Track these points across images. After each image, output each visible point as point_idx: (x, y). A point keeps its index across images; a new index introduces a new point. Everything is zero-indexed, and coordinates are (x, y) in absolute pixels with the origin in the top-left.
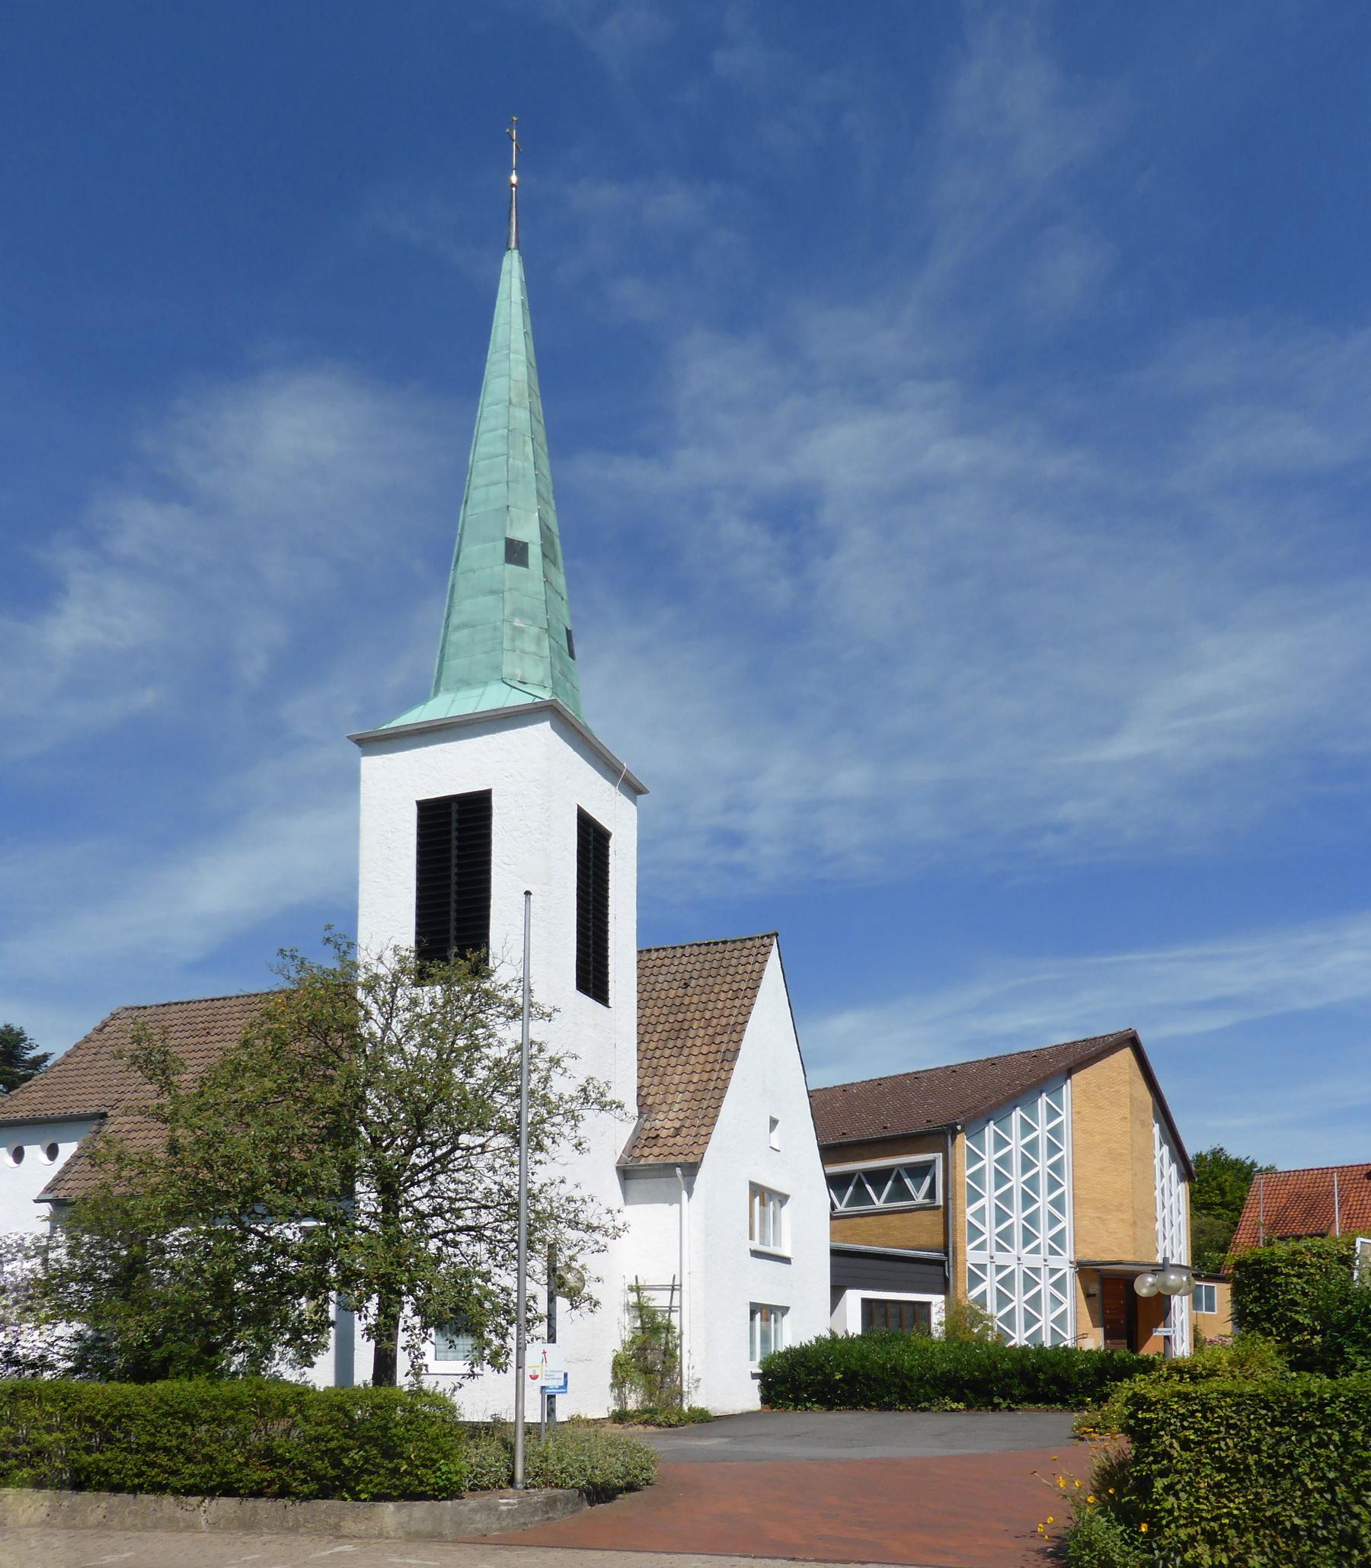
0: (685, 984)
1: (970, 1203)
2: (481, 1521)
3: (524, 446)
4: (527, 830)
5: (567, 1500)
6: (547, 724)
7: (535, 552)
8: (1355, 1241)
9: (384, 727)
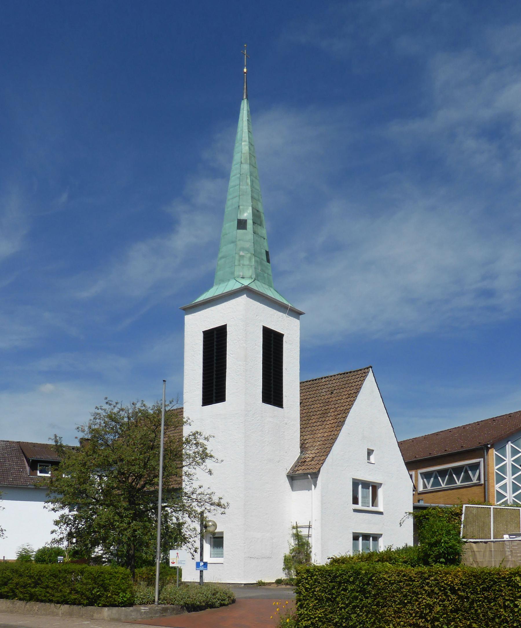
0: (332, 392)
1: (498, 482)
2: (134, 615)
3: (247, 180)
4: (238, 340)
5: (174, 609)
6: (245, 295)
7: (250, 223)
8: (463, 506)
9: (193, 303)
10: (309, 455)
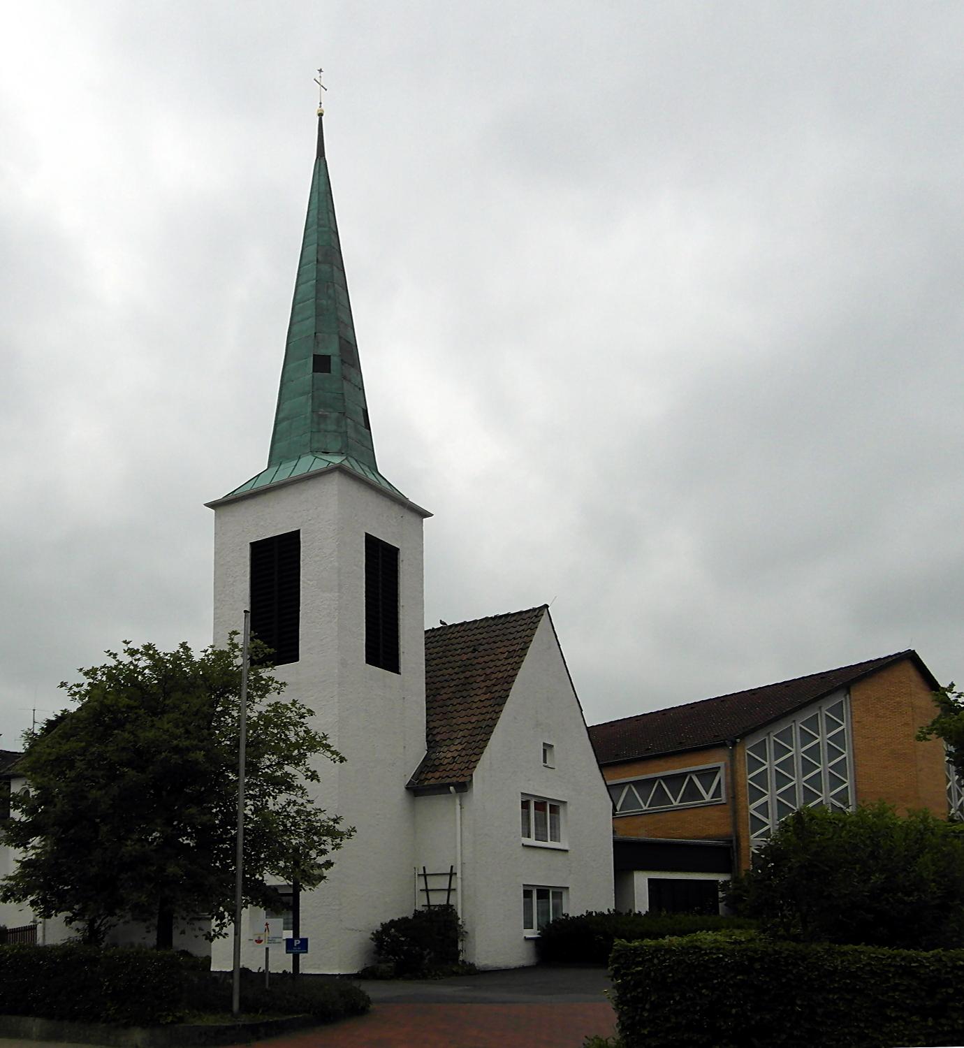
0: (474, 649)
10: (446, 754)
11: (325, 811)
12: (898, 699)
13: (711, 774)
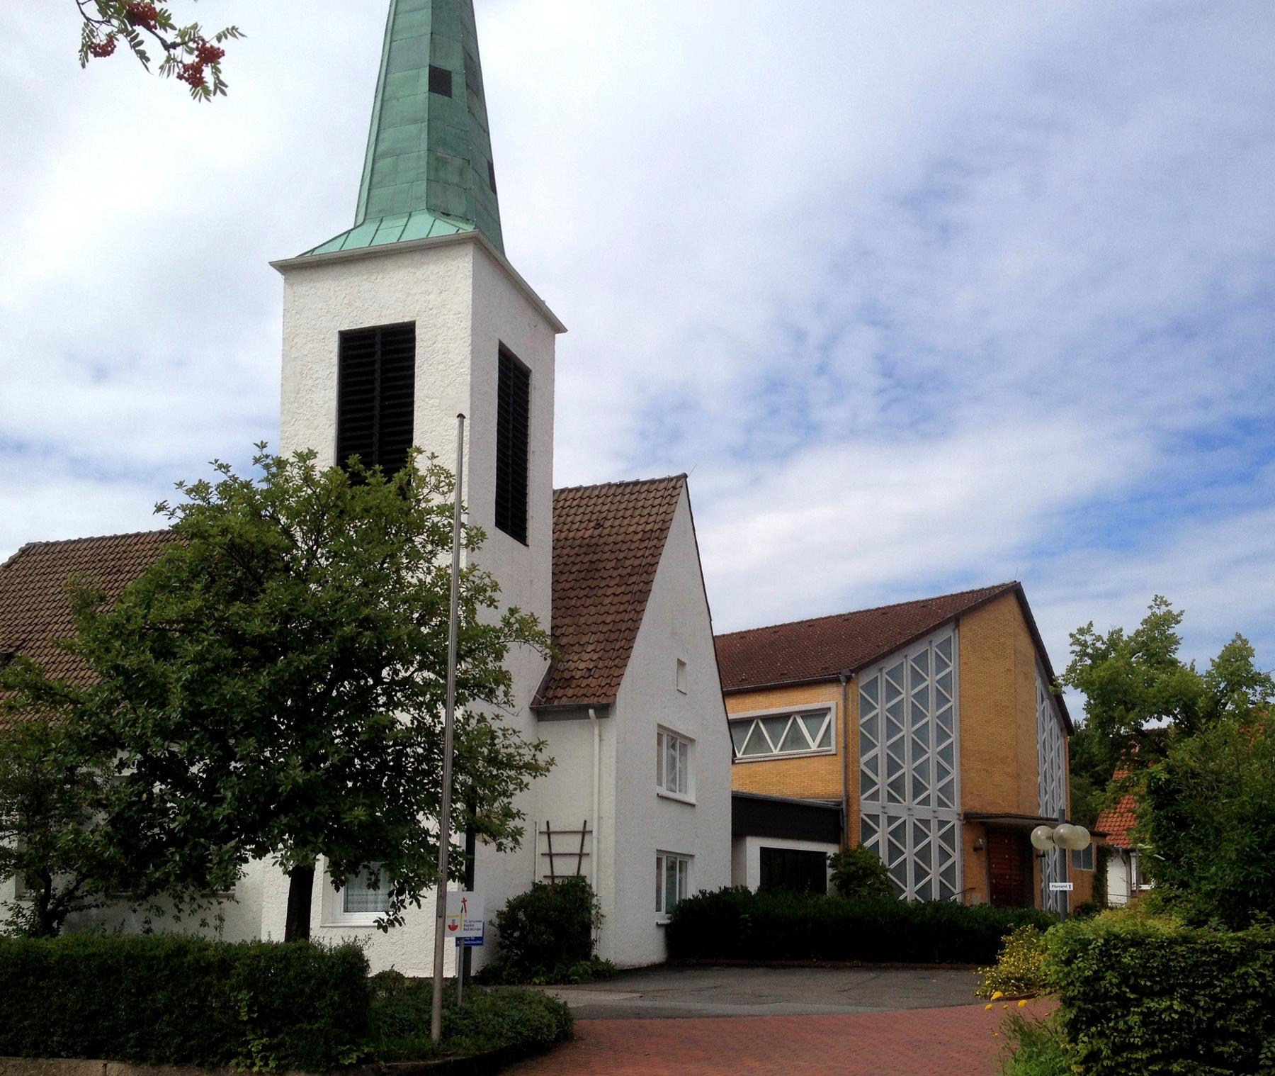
11: (519, 732)
12: (1002, 640)
13: (816, 715)
